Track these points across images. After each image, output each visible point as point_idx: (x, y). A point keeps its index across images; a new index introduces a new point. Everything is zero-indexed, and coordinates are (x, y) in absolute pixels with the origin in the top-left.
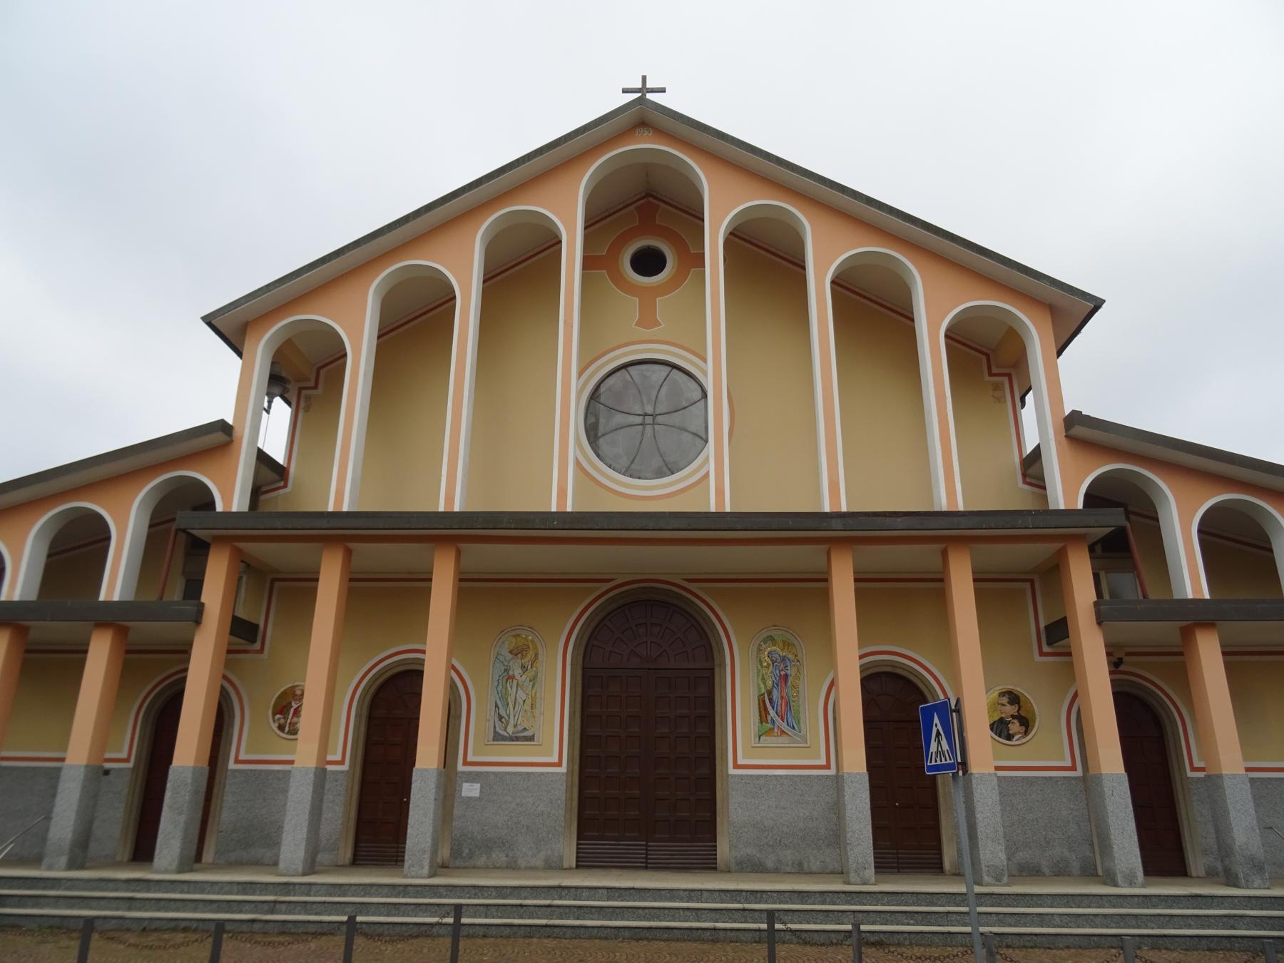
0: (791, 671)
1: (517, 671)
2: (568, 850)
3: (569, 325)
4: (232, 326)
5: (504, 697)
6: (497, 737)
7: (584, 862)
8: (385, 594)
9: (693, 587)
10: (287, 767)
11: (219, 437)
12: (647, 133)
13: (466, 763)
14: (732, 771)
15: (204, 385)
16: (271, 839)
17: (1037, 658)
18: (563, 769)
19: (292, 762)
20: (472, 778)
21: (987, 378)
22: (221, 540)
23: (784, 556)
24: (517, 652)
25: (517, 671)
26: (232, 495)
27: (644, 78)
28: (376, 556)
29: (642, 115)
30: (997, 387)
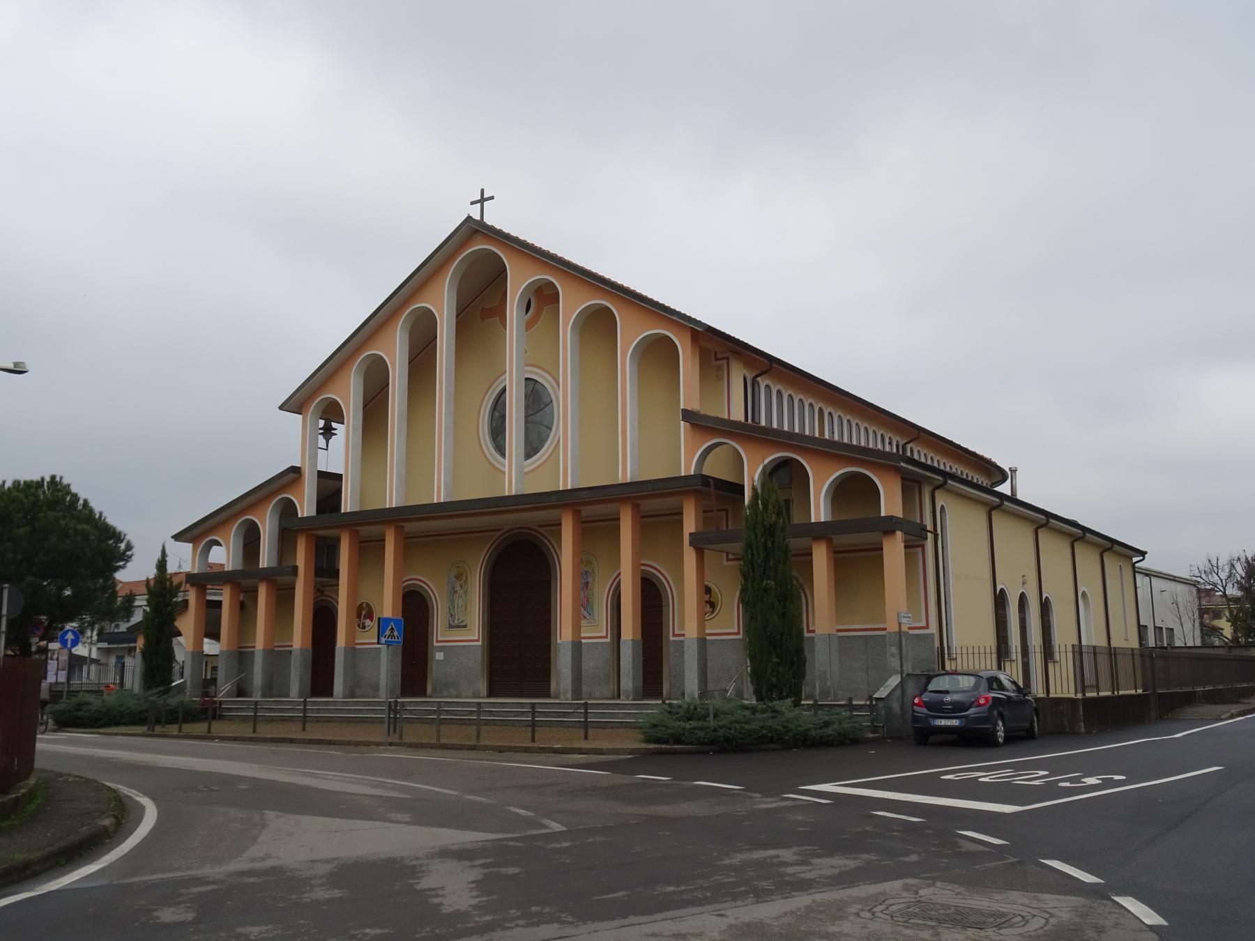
0: (590, 580)
1: (458, 588)
2: (483, 687)
3: (441, 383)
4: (295, 404)
5: (452, 603)
6: (451, 627)
7: (490, 695)
8: (411, 546)
9: (540, 530)
10: (884, 633)
11: (291, 476)
12: (479, 238)
13: (674, 635)
14: (672, 638)
15: (283, 443)
16: (377, 688)
17: (726, 563)
18: (608, 640)
19: (885, 629)
20: (441, 649)
21: (714, 363)
22: (302, 531)
23: (595, 508)
24: (458, 577)
25: (458, 588)
26: (306, 507)
27: (482, 191)
28: (365, 531)
29: (473, 229)
30: (720, 369)
